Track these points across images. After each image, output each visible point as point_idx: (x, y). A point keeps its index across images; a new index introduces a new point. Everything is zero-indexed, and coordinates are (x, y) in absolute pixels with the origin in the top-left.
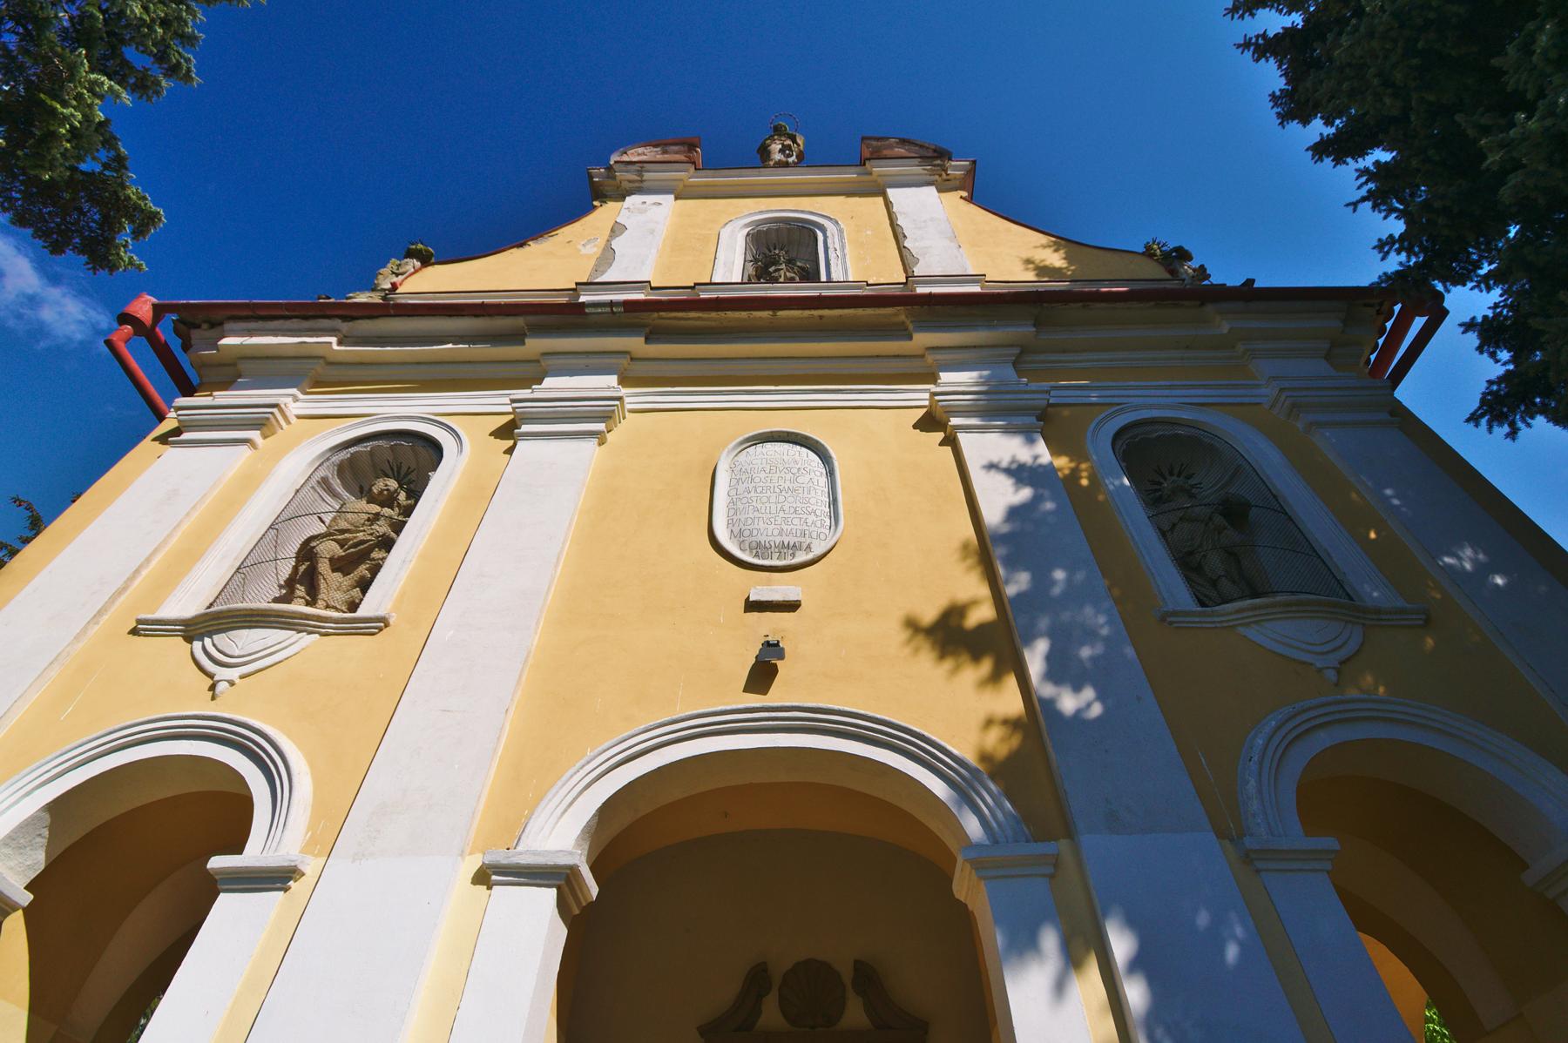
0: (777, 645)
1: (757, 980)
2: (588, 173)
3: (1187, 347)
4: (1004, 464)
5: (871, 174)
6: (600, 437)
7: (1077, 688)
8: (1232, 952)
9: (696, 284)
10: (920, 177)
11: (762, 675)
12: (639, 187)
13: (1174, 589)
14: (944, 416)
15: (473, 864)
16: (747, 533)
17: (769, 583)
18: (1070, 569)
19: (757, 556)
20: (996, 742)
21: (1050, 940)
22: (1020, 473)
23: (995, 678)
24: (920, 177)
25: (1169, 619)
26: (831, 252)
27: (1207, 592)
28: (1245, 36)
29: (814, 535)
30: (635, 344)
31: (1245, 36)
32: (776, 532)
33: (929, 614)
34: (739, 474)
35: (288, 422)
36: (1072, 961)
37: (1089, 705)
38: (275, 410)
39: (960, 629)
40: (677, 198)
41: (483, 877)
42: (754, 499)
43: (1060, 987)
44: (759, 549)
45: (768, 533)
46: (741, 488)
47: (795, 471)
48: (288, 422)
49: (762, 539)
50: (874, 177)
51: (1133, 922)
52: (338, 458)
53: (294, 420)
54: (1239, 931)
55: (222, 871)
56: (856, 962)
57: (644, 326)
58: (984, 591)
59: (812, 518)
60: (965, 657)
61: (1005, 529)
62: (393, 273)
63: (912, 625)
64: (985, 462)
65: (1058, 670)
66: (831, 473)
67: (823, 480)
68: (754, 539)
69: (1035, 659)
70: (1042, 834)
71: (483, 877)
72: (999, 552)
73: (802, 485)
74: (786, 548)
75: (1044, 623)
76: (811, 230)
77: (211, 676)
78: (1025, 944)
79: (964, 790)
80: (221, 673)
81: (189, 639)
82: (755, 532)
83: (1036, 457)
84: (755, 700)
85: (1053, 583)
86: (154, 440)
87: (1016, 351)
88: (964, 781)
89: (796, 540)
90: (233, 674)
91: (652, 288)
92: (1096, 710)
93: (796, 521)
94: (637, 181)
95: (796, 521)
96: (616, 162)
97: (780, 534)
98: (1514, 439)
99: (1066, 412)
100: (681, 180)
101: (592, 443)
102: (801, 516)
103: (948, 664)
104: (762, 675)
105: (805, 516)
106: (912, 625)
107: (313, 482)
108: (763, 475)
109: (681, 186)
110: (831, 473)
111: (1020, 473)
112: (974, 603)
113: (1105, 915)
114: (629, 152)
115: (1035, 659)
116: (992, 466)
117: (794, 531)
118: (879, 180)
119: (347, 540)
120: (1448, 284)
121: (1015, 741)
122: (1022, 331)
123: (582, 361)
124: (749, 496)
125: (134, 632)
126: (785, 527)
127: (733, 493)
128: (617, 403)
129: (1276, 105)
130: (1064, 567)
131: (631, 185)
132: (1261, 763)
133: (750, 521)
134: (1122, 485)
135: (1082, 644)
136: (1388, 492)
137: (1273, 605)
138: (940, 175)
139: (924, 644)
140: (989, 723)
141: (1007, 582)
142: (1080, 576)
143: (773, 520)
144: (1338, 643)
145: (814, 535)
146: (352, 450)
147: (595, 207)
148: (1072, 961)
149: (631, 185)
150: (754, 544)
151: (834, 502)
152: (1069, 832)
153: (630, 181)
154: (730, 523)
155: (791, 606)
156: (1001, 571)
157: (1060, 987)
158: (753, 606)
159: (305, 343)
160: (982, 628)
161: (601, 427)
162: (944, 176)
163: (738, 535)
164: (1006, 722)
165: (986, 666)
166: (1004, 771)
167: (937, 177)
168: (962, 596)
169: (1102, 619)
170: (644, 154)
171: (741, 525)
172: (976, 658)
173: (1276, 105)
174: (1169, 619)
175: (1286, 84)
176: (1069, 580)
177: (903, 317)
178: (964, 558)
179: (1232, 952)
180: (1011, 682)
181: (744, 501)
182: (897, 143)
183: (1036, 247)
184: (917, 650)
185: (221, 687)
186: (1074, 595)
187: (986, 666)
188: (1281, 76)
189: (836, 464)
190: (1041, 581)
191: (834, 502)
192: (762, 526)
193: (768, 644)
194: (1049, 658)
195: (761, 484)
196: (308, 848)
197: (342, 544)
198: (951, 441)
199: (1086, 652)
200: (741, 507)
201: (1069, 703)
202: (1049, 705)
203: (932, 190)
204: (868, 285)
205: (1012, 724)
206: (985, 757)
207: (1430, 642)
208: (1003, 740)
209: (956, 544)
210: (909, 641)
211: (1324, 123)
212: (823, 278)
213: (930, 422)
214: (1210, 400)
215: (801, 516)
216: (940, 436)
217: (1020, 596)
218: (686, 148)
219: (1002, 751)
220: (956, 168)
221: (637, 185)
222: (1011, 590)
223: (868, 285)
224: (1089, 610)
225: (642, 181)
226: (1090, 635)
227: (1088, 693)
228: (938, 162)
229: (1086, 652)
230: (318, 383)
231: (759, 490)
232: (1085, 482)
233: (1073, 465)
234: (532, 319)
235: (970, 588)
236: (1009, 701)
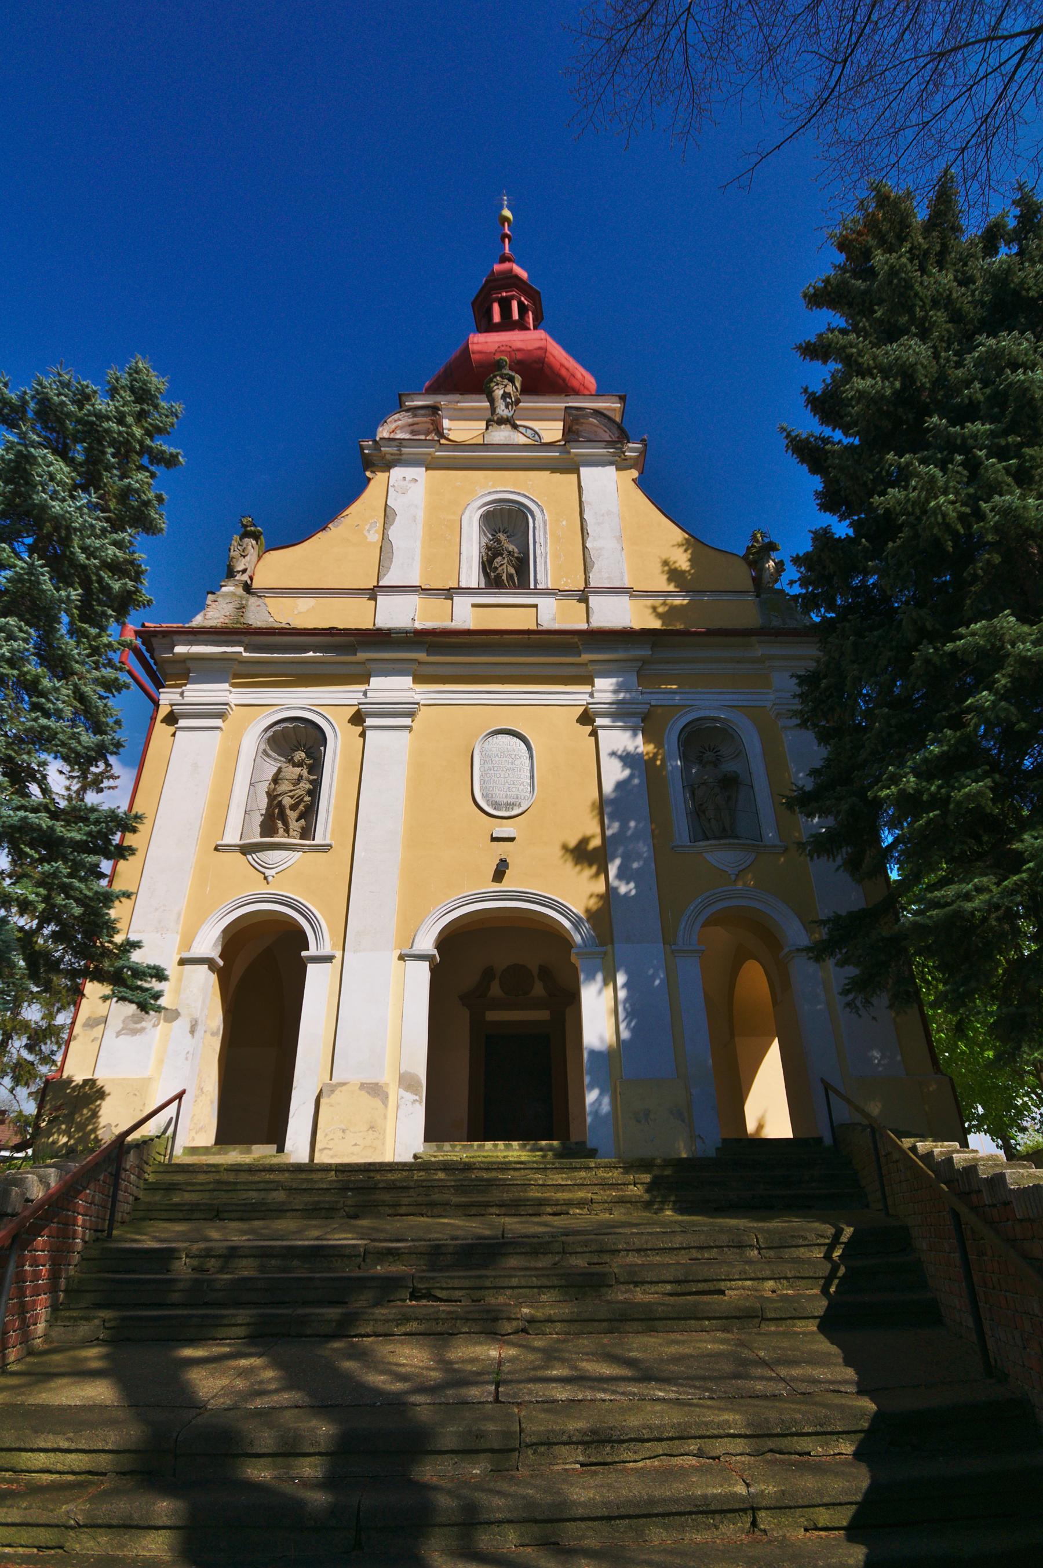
1: (488, 974)
2: (360, 446)
3: (738, 662)
4: (619, 753)
5: (569, 452)
6: (409, 728)
7: (628, 883)
8: (657, 982)
9: (451, 588)
10: (605, 458)
11: (499, 875)
12: (399, 459)
13: (681, 827)
14: (593, 717)
15: (397, 953)
16: (490, 796)
17: (501, 826)
18: (638, 822)
19: (495, 809)
20: (593, 904)
21: (599, 977)
22: (627, 759)
23: (597, 875)
24: (605, 458)
26: (538, 545)
33: (573, 843)
34: (486, 759)
35: (232, 710)
36: (605, 983)
37: (631, 890)
38: (227, 707)
39: (585, 849)
40: (427, 469)
41: (401, 958)
43: (600, 992)
44: (496, 805)
45: (501, 797)
46: (486, 766)
48: (232, 710)
49: (497, 799)
50: (572, 456)
51: (628, 972)
52: (270, 733)
53: (234, 707)
54: (662, 976)
55: (305, 957)
56: (540, 966)
57: (426, 643)
58: (598, 830)
59: (522, 787)
60: (586, 865)
61: (613, 796)
62: (242, 555)
63: (565, 847)
64: (610, 751)
65: (621, 875)
66: (531, 757)
67: (528, 762)
69: (613, 869)
70: (602, 944)
71: (401, 958)
72: (608, 810)
74: (510, 806)
75: (620, 850)
76: (524, 513)
78: (591, 977)
79: (576, 924)
80: (268, 872)
81: (244, 854)
83: (636, 748)
84: (497, 887)
85: (629, 828)
86: (162, 721)
87: (640, 664)
88: (577, 923)
90: (272, 872)
91: (422, 590)
92: (633, 892)
93: (514, 790)
94: (397, 454)
95: (514, 790)
96: (381, 439)
97: (506, 797)
99: (660, 710)
100: (430, 454)
101: (405, 733)
103: (578, 868)
104: (499, 875)
106: (565, 847)
107: (260, 754)
109: (430, 458)
110: (531, 757)
111: (627, 759)
112: (593, 836)
113: (618, 971)
114: (388, 421)
115: (613, 869)
116: (613, 754)
118: (576, 458)
119: (294, 796)
121: (601, 903)
122: (645, 652)
123: (390, 666)
125: (216, 849)
127: (482, 769)
128: (417, 706)
129: (817, 498)
130: (636, 820)
131: (393, 457)
132: (689, 917)
134: (677, 764)
135: (634, 861)
137: (720, 845)
138: (620, 457)
139: (568, 856)
140: (591, 896)
141: (608, 828)
142: (641, 825)
144: (742, 862)
146: (273, 729)
147: (369, 480)
148: (605, 983)
149: (393, 457)
151: (532, 777)
152: (612, 942)
153: (392, 454)
154: (482, 789)
155: (511, 839)
156: (606, 821)
157: (600, 992)
158: (494, 839)
159: (226, 652)
160: (595, 849)
161: (407, 721)
162: (623, 457)
163: (485, 796)
164: (598, 896)
165: (594, 869)
166: (592, 916)
167: (617, 458)
168: (589, 833)
169: (645, 849)
170: (400, 420)
172: (590, 865)
173: (817, 498)
176: (636, 826)
177: (577, 640)
178: (592, 811)
179: (657, 982)
180: (602, 877)
182: (591, 414)
183: (674, 546)
184: (566, 861)
185: (270, 879)
186: (637, 835)
187: (594, 869)
189: (534, 752)
190: (624, 827)
191: (532, 777)
192: (497, 792)
193: (501, 860)
194: (620, 868)
196: (334, 947)
197: (292, 797)
198: (594, 733)
199: (635, 865)
201: (623, 889)
202: (615, 889)
203: (613, 468)
204: (560, 591)
205: (600, 897)
206: (587, 911)
207: (782, 859)
208: (596, 903)
209: (589, 803)
210: (563, 856)
212: (532, 587)
213: (586, 718)
214: (740, 703)
216: (589, 728)
217: (613, 835)
218: (431, 412)
219: (594, 908)
220: (632, 450)
221: (397, 457)
222: (609, 833)
223: (560, 591)
224: (641, 844)
225: (401, 455)
226: (638, 857)
227: (632, 885)
228: (619, 446)
229: (635, 865)
230: (236, 676)
232: (658, 763)
233: (655, 750)
234: (359, 638)
235: (590, 827)
236: (600, 887)
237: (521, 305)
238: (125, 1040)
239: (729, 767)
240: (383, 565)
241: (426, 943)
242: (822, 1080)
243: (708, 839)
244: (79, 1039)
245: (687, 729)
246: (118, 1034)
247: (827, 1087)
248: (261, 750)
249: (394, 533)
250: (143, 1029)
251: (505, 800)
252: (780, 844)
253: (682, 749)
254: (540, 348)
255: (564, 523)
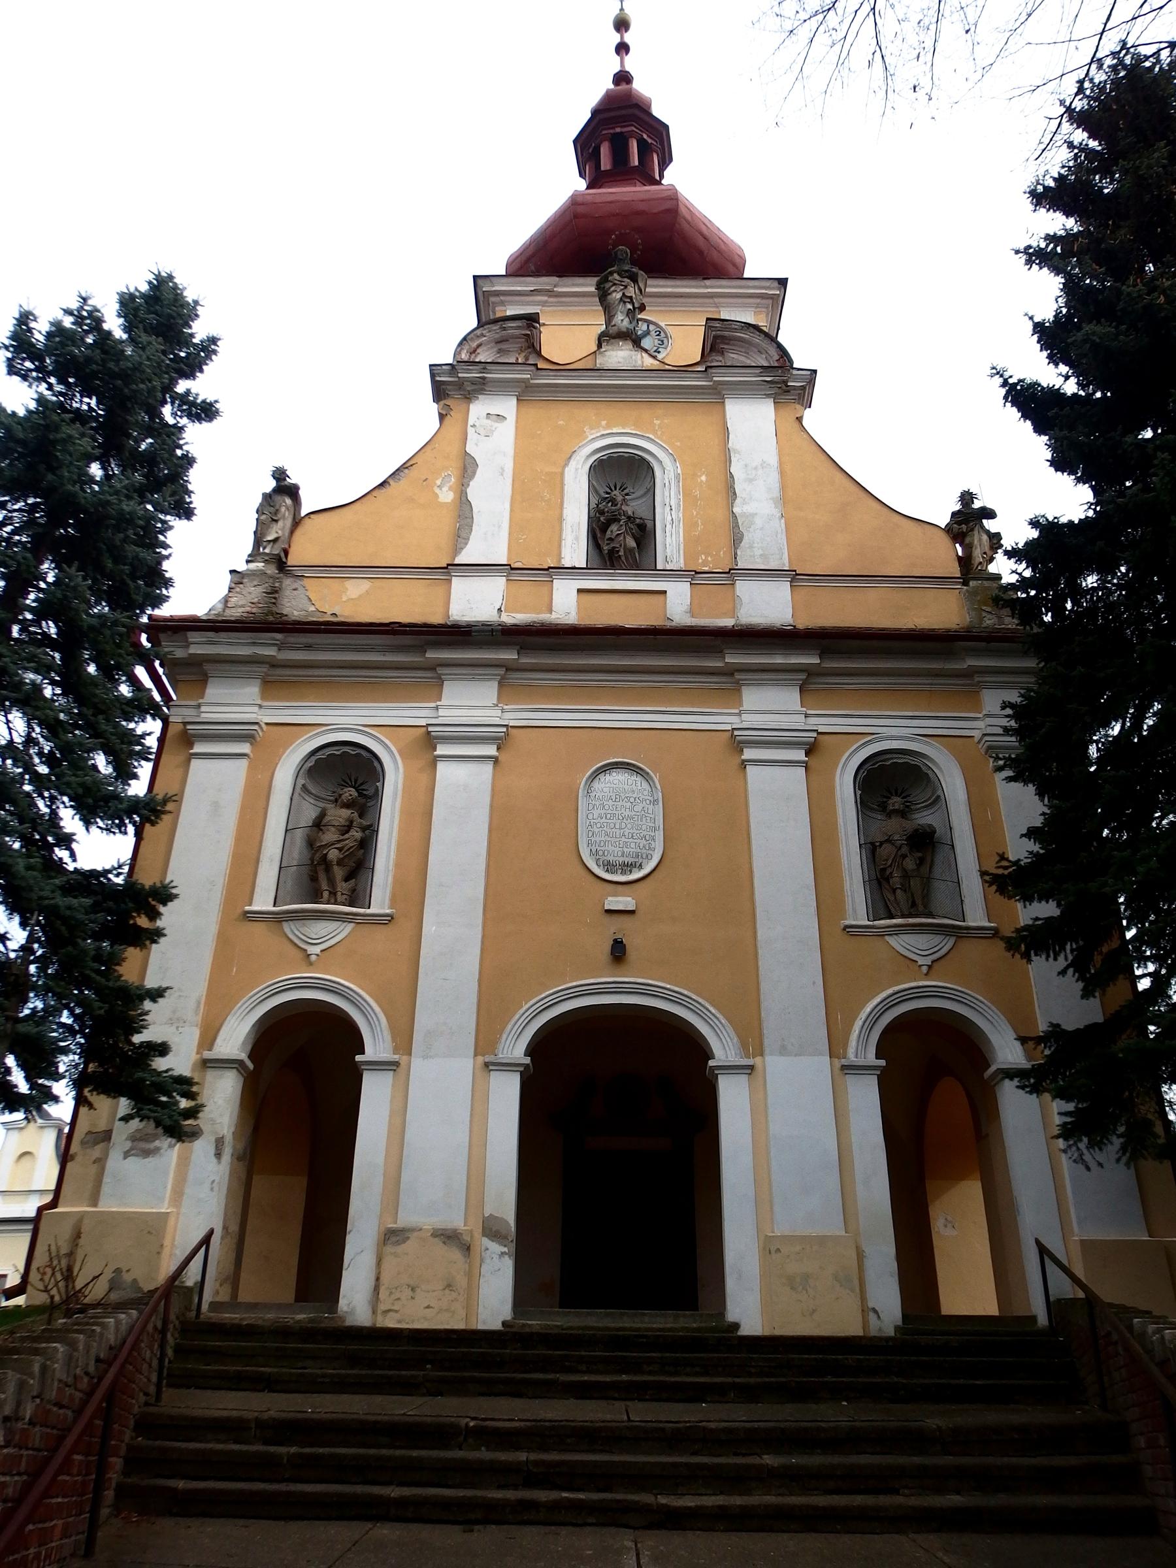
0: (622, 942)
13: (857, 908)
16: (601, 853)
19: (607, 871)
25: (848, 930)
27: (881, 905)
28: (1029, 269)
29: (644, 856)
30: (510, 655)
31: (1029, 269)
32: (620, 854)
42: (605, 824)
44: (609, 867)
47: (632, 800)
49: (611, 858)
68: (605, 858)
73: (638, 814)
74: (628, 867)
77: (306, 950)
82: (606, 853)
89: (633, 860)
95: (633, 845)
98: (967, 498)
102: (636, 841)
105: (639, 841)
108: (611, 803)
117: (631, 853)
120: (1081, 1294)
124: (602, 821)
126: (625, 850)
133: (602, 844)
136: (1095, 844)
143: (617, 843)
145: (644, 856)
150: (606, 862)
171: (597, 847)
174: (848, 930)
175: (1095, 997)
181: (599, 825)
188: (1036, 257)
193: (615, 941)
195: (611, 812)
197: (340, 849)
200: (597, 830)
211: (1050, 357)
215: (636, 841)
231: (609, 816)
237: (642, 145)
238: (134, 1163)
239: (925, 818)
240: (457, 551)
241: (516, 1048)
242: (1038, 1242)
243: (891, 917)
244: (79, 1159)
245: (868, 766)
246: (126, 1155)
247: (1043, 1251)
248: (299, 786)
249: (474, 492)
250: (157, 1150)
251: (621, 860)
252: (987, 924)
253: (859, 792)
254: (668, 211)
255: (703, 478)
